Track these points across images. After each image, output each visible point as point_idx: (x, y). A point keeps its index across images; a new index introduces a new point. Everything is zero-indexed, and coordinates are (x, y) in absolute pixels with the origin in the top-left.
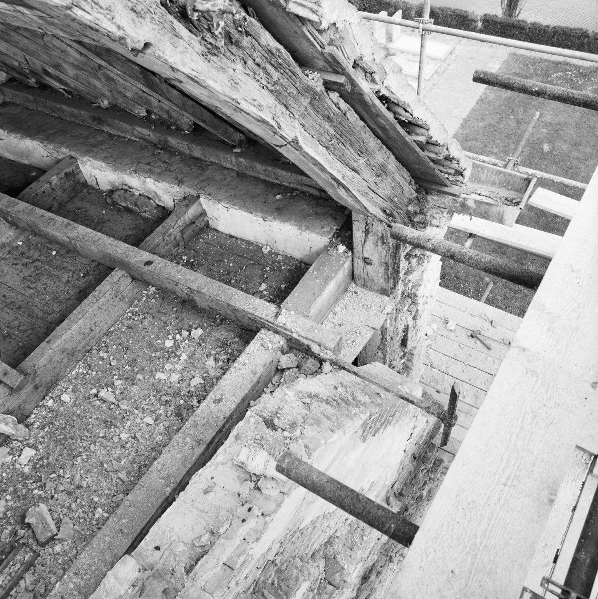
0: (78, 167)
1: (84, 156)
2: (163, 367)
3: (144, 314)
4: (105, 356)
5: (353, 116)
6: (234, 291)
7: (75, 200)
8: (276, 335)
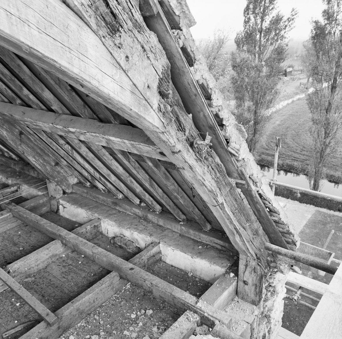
0: (100, 224)
1: (105, 218)
2: (128, 329)
3: (122, 299)
4: (97, 318)
5: (246, 202)
6: (175, 288)
7: (95, 239)
8: (195, 314)
